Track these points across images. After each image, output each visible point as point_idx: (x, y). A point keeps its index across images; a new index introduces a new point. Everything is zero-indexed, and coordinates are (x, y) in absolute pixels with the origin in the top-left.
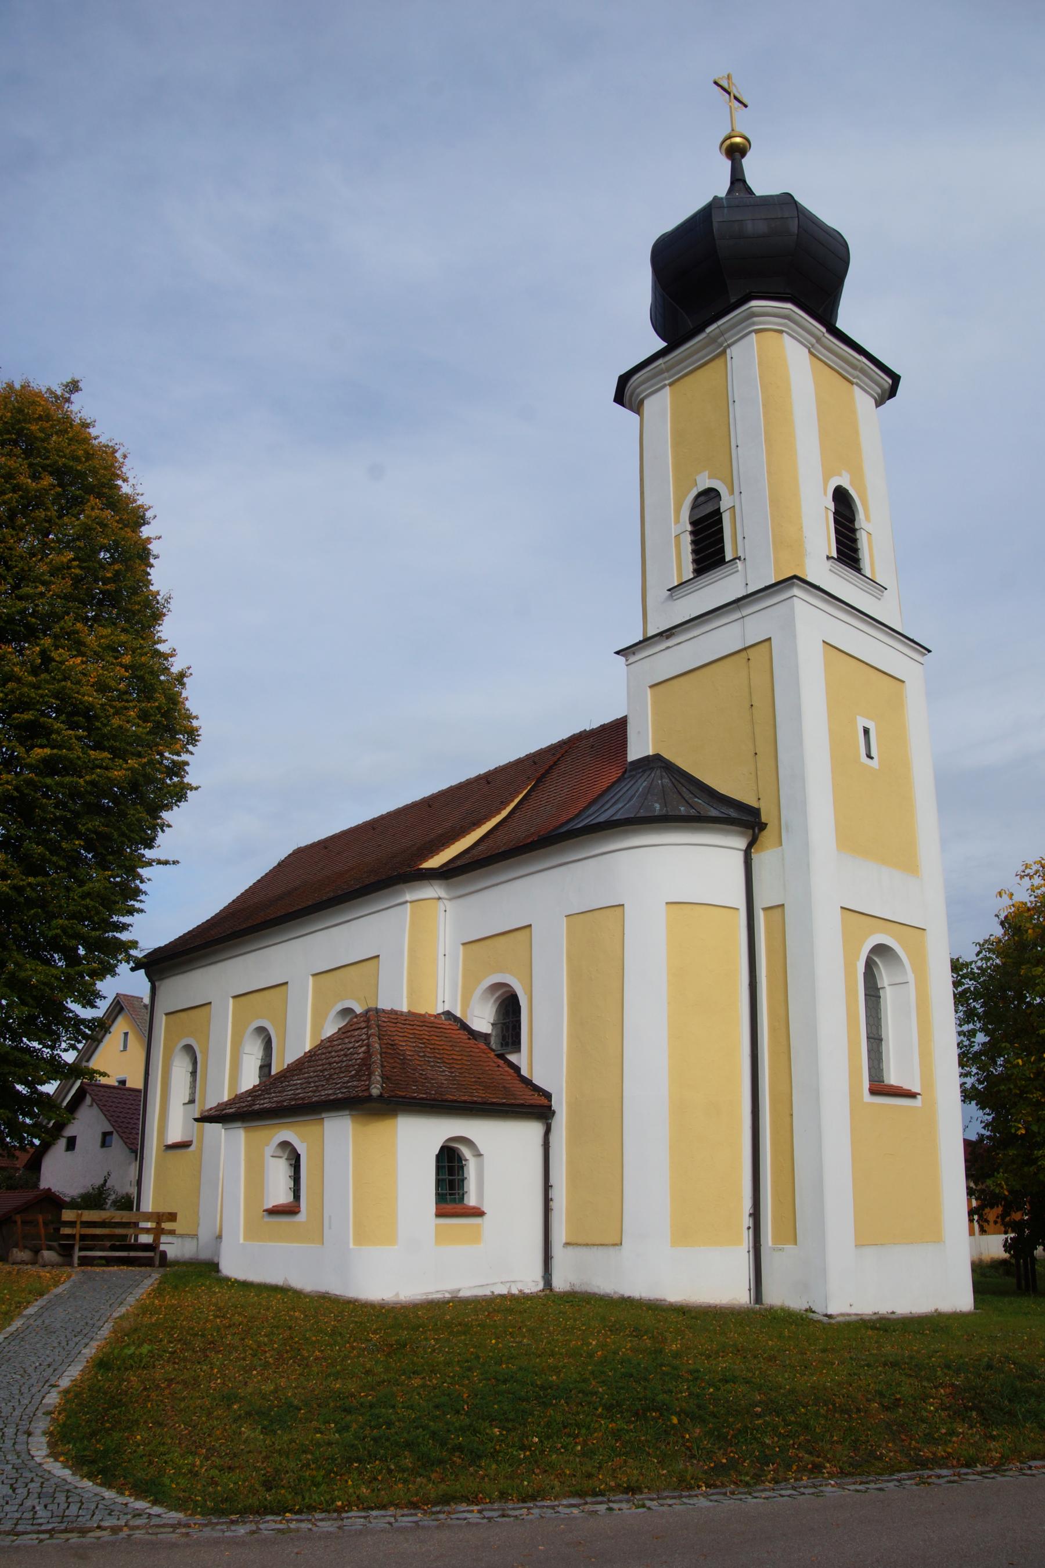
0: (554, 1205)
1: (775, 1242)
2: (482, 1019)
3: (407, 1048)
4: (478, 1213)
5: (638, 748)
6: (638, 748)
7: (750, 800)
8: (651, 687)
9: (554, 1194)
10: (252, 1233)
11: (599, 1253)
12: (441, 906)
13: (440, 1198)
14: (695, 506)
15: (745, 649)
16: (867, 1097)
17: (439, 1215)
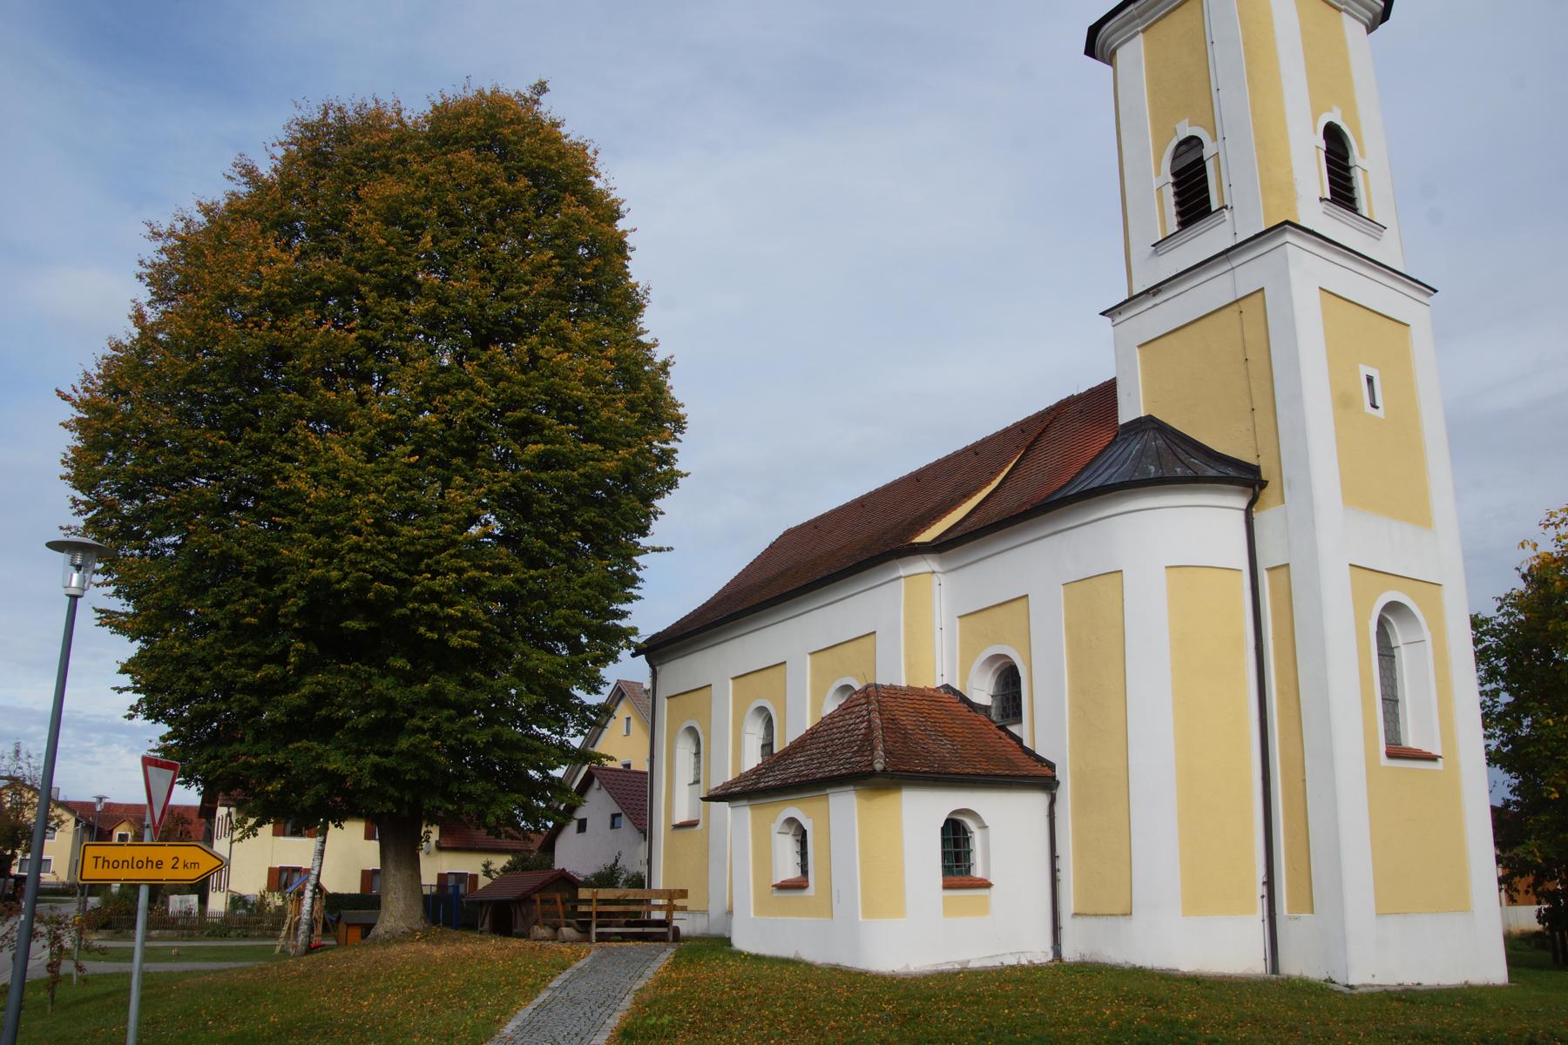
0: (1061, 875)
2: (982, 692)
3: (907, 721)
4: (985, 885)
5: (1130, 409)
6: (1130, 409)
7: (1249, 458)
9: (1060, 864)
10: (762, 907)
12: (935, 579)
13: (947, 870)
14: (1176, 156)
15: (1237, 301)
16: (1384, 761)
17: (946, 887)
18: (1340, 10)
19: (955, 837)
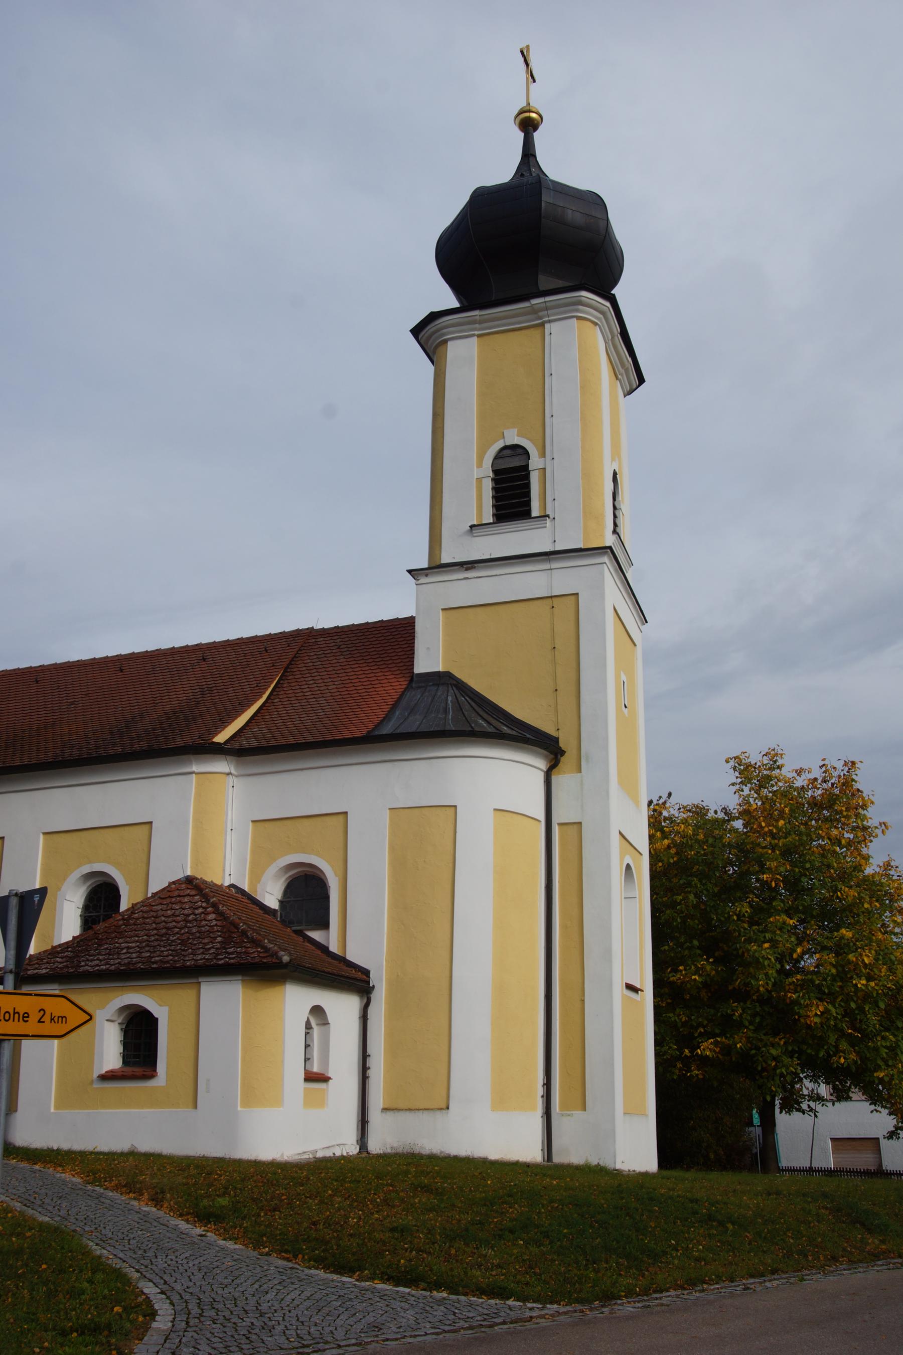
0: (371, 1073)
1: (561, 1108)
5: (427, 661)
6: (427, 661)
7: (549, 729)
8: (443, 610)
9: (371, 1062)
11: (425, 1116)
12: (231, 780)
14: (498, 457)
15: (552, 597)
18: (617, 378)
19: (140, 1033)
